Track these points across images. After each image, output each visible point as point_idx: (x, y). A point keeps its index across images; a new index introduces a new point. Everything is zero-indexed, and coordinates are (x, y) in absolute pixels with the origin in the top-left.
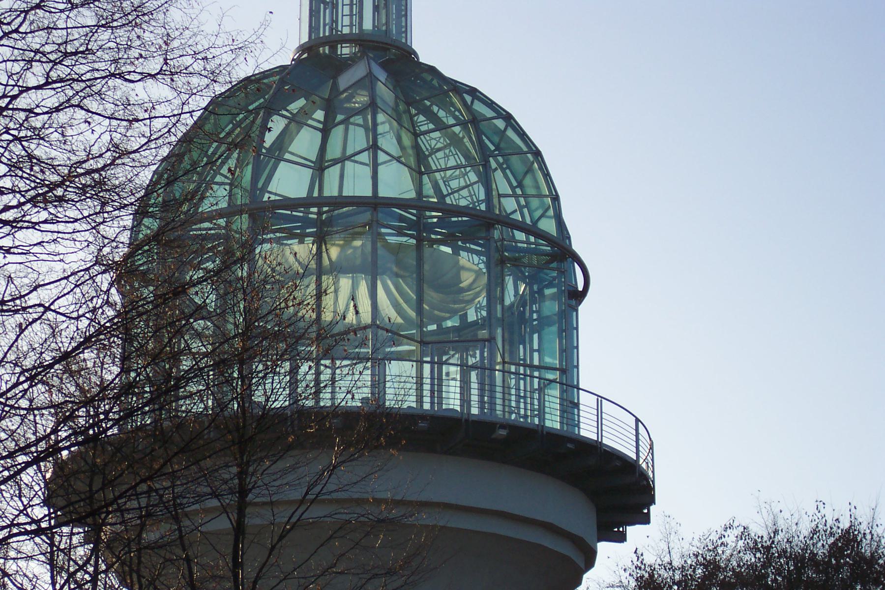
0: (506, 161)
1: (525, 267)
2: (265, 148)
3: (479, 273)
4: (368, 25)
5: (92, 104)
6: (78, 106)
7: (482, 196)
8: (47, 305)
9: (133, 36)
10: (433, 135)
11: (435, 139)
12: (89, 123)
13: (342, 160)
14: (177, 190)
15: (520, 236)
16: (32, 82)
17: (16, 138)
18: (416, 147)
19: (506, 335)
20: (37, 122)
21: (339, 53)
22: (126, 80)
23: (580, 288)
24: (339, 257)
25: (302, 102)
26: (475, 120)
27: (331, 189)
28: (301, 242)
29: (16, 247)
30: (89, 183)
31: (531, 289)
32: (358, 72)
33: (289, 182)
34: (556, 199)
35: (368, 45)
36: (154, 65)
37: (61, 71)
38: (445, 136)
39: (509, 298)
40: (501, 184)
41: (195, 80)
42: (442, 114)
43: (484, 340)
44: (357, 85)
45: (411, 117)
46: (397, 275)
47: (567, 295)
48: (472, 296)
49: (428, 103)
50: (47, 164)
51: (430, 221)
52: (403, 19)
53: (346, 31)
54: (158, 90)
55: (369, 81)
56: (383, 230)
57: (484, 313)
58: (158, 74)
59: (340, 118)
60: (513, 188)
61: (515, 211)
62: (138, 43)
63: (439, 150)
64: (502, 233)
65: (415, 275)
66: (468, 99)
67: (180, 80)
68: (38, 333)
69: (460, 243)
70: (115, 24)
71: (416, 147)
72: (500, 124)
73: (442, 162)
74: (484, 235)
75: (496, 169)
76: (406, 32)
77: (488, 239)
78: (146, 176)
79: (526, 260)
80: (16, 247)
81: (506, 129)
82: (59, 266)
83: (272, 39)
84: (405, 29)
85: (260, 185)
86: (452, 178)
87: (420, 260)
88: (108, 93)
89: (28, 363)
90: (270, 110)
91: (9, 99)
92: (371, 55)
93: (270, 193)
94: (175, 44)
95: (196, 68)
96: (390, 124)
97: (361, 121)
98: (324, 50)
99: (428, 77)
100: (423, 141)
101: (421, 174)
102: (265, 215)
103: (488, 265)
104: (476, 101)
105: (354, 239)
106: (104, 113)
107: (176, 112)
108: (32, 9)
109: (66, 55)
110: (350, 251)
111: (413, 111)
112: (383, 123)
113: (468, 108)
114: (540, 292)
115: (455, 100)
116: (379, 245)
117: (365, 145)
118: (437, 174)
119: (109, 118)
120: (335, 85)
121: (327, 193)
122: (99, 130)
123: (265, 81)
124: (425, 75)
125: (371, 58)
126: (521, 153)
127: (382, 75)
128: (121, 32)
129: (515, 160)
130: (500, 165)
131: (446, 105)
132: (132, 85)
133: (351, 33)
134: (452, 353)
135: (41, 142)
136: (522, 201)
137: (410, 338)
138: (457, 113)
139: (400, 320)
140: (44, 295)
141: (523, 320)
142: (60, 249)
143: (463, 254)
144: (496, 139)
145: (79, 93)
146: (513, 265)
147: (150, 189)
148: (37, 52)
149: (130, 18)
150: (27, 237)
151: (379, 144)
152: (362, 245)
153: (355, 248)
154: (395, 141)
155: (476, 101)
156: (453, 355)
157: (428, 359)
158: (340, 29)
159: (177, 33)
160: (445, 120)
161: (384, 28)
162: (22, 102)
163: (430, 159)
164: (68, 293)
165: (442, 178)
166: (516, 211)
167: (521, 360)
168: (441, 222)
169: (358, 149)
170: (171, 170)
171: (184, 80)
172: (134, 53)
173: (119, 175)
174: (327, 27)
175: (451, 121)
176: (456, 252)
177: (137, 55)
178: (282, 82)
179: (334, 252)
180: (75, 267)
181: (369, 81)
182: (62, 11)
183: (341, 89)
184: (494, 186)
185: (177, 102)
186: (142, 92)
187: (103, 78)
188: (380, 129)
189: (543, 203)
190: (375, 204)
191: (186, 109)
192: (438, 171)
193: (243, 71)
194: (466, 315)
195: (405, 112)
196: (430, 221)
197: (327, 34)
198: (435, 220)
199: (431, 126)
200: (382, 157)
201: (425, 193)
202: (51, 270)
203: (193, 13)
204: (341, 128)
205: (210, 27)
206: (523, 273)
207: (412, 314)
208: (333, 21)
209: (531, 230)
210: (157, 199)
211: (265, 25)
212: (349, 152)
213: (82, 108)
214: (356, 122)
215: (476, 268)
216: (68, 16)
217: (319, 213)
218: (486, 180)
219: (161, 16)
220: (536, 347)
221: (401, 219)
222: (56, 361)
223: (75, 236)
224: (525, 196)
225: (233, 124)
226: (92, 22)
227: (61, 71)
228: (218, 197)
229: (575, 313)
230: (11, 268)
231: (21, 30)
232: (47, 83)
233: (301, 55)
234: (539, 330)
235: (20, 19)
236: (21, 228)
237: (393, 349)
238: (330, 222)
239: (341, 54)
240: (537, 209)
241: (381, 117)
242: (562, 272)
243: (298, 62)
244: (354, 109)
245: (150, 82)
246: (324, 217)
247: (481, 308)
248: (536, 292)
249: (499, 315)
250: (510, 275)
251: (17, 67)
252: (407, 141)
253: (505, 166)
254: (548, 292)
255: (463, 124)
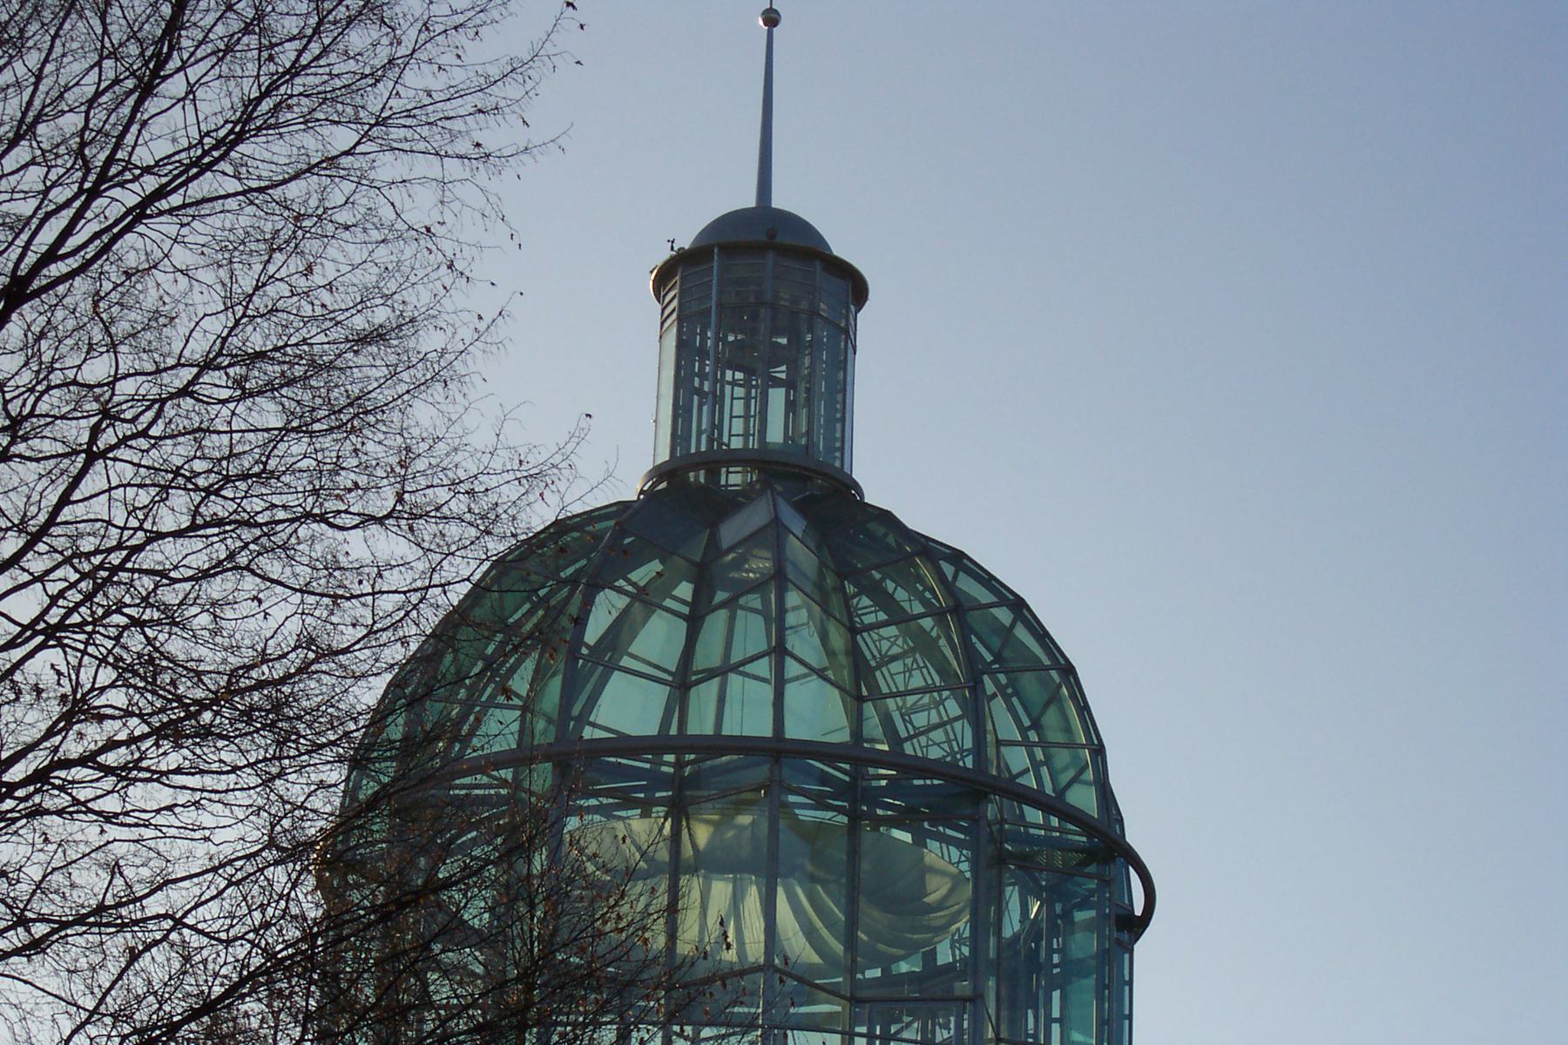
0: (1012, 682)
1: (1041, 870)
2: (588, 646)
3: (958, 879)
4: (775, 434)
5: (273, 567)
6: (247, 568)
7: (968, 744)
8: (178, 916)
9: (348, 446)
10: (884, 632)
11: (888, 640)
12: (260, 602)
13: (725, 670)
14: (432, 711)
15: (1034, 815)
16: (167, 523)
17: (137, 623)
18: (854, 652)
19: (1004, 991)
20: (170, 596)
21: (723, 482)
22: (332, 525)
23: (1138, 911)
24: (710, 843)
25: (655, 566)
26: (959, 608)
27: (701, 723)
28: (646, 814)
29: (127, 814)
30: (258, 704)
31: (1051, 910)
32: (755, 516)
33: (627, 708)
34: (1099, 751)
35: (771, 468)
36: (382, 502)
37: (216, 507)
38: (906, 634)
39: (1012, 925)
40: (1003, 723)
41: (453, 530)
42: (901, 595)
43: (964, 1000)
44: (753, 539)
45: (847, 599)
46: (814, 879)
47: (1117, 923)
48: (943, 921)
49: (877, 576)
50: (186, 668)
51: (874, 783)
52: (838, 426)
53: (736, 443)
54: (390, 545)
55: (774, 533)
56: (792, 798)
57: (966, 950)
58: (389, 516)
59: (721, 596)
60: (1023, 730)
61: (1026, 771)
62: (355, 462)
63: (894, 658)
64: (1001, 810)
65: (844, 880)
66: (948, 569)
67: (427, 529)
68: (158, 965)
69: (926, 825)
70: (317, 427)
71: (854, 652)
72: (1004, 615)
73: (899, 679)
74: (968, 812)
75: (994, 696)
76: (842, 449)
77: (975, 820)
78: (369, 694)
79: (1042, 859)
80: (127, 814)
81: (1013, 625)
82: (201, 849)
83: (590, 464)
84: (840, 442)
85: (576, 711)
86: (916, 709)
87: (854, 853)
88: (300, 547)
89: (141, 1016)
90: (595, 584)
91: (125, 553)
92: (779, 488)
93: (594, 725)
94: (420, 465)
95: (455, 509)
96: (809, 611)
97: (757, 604)
98: (697, 477)
99: (880, 530)
100: (867, 642)
101: (861, 699)
102: (583, 765)
103: (975, 864)
104: (961, 574)
105: (739, 812)
106: (292, 582)
107: (419, 584)
108: (172, 396)
109: (227, 479)
110: (730, 834)
111: (851, 589)
112: (795, 608)
113: (948, 586)
114: (1067, 916)
115: (926, 572)
116: (782, 824)
117: (763, 647)
118: (890, 702)
119: (301, 591)
120: (713, 540)
121: (693, 729)
122: (278, 614)
123: (590, 528)
124: (872, 526)
125: (780, 494)
126: (1038, 667)
127: (796, 524)
128: (327, 441)
129: (1028, 681)
130: (1001, 689)
131: (910, 581)
132: (339, 535)
133: (746, 449)
134: (907, 1019)
135: (175, 629)
136: (1039, 754)
137: (833, 992)
138: (928, 595)
139: (816, 959)
140: (178, 898)
141: (1034, 964)
142: (206, 820)
143: (933, 845)
144: (996, 643)
145: (251, 543)
146: (1019, 867)
147: (380, 715)
148: (177, 472)
149: (344, 418)
150: (144, 795)
151: (789, 646)
152: (753, 822)
153: (741, 828)
154: (816, 640)
155: (961, 574)
156: (909, 1025)
157: (863, 1030)
158: (725, 440)
159: (424, 446)
160: (906, 606)
161: (803, 441)
162: (150, 558)
163: (878, 674)
164: (212, 898)
165: (899, 709)
166: (1027, 770)
167: (1029, 1036)
168: (894, 787)
169: (751, 652)
170: (416, 684)
171: (432, 528)
172: (345, 479)
173: (314, 690)
174: (704, 437)
175: (918, 608)
176: (920, 841)
177: (350, 485)
178: (621, 531)
179: (703, 834)
180: (227, 850)
181: (774, 533)
182: (223, 402)
183: (725, 545)
184: (989, 727)
185: (421, 566)
186: (357, 546)
187: (292, 521)
188: (791, 619)
189: (1076, 758)
190: (778, 751)
191: (436, 580)
192: (892, 695)
193: (539, 516)
194: (933, 953)
195: (835, 589)
196: (874, 783)
197: (703, 449)
198: (883, 783)
199: (882, 616)
200: (792, 669)
201: (866, 732)
202: (190, 855)
203: (454, 411)
204: (723, 614)
205: (482, 439)
206: (1036, 881)
207: (838, 948)
208: (713, 426)
209: (1054, 806)
210: (396, 730)
211: (577, 437)
212: (736, 657)
213: (253, 573)
214: (751, 605)
215: (953, 869)
216: (233, 413)
217: (679, 765)
218: (976, 713)
219: (396, 416)
220: (1056, 1013)
221: (824, 779)
222: (194, 1015)
223: (230, 797)
224: (1044, 744)
225: (532, 602)
226: (276, 422)
227: (216, 507)
228: (499, 730)
229: (1127, 956)
230: (119, 849)
231: (151, 433)
232: (194, 527)
233: (654, 485)
234: (1062, 983)
235: (150, 415)
236: (136, 780)
237: (803, 1010)
238: (696, 780)
239: (727, 485)
240: (1066, 768)
241: (793, 598)
242: (1106, 883)
243: (649, 496)
244: (746, 581)
245: (374, 528)
246: (686, 772)
247: (961, 941)
248: (1059, 916)
249: (992, 954)
250: (1013, 884)
251: (144, 498)
252: (838, 640)
253: (1010, 691)
254: (1080, 916)
255: (938, 615)
